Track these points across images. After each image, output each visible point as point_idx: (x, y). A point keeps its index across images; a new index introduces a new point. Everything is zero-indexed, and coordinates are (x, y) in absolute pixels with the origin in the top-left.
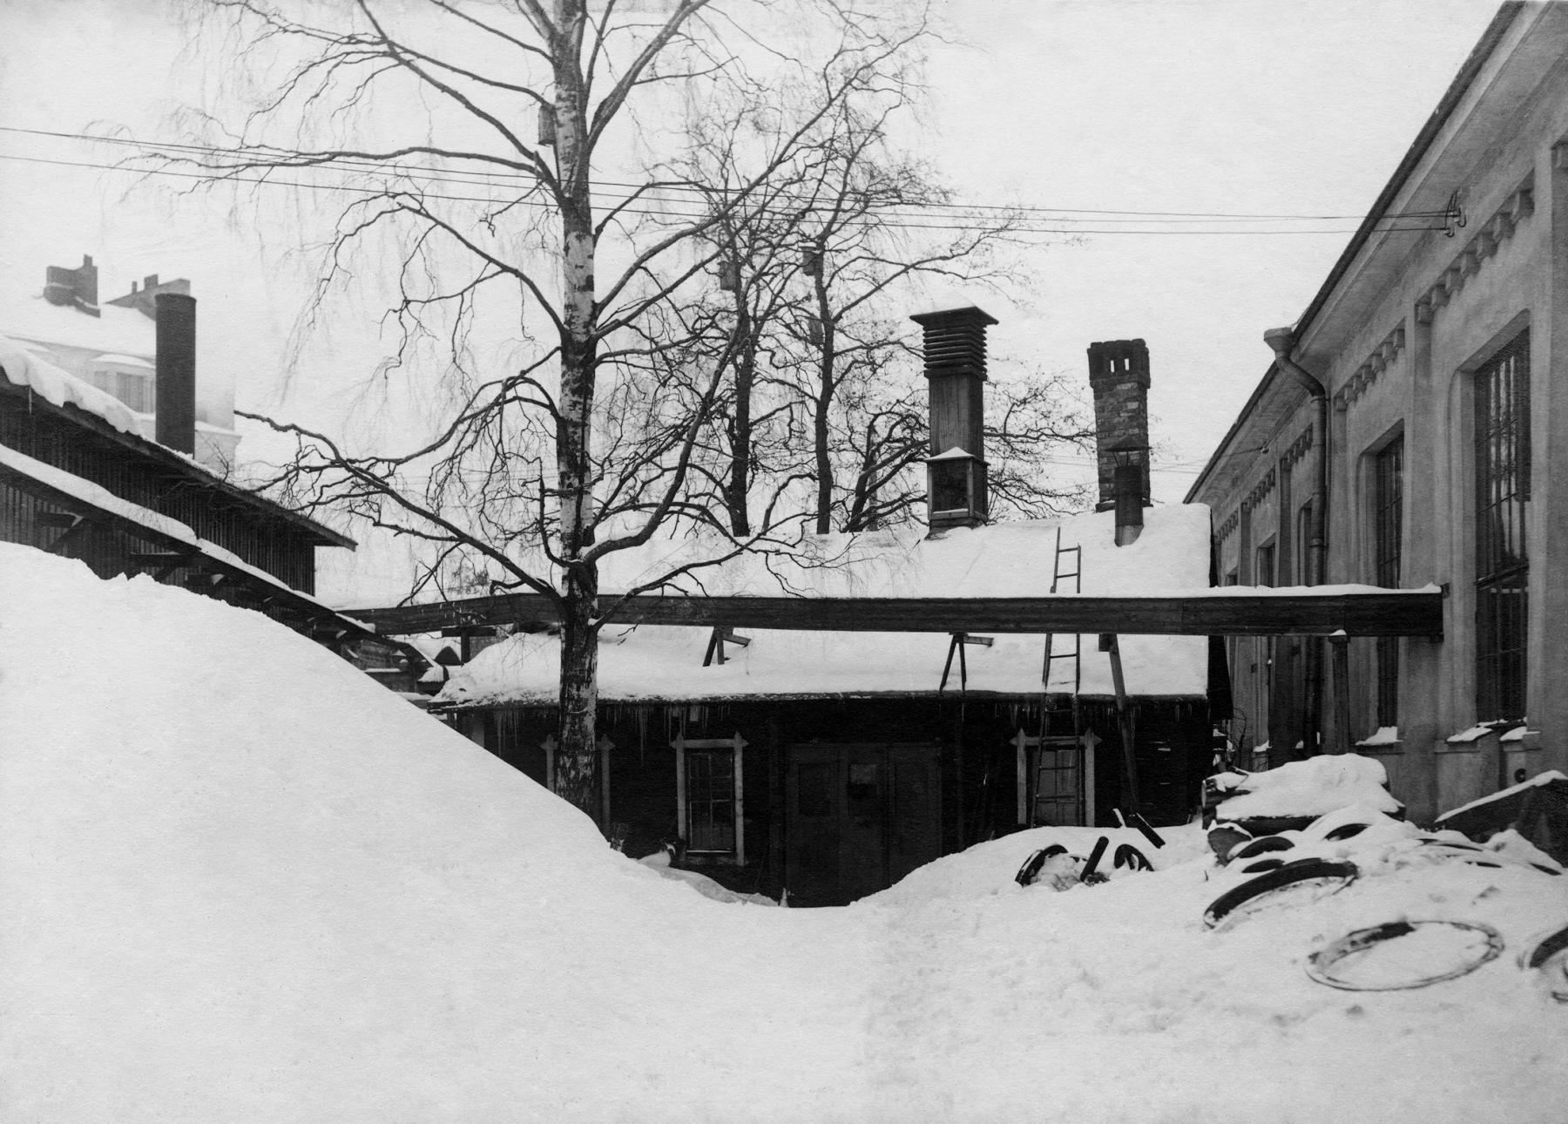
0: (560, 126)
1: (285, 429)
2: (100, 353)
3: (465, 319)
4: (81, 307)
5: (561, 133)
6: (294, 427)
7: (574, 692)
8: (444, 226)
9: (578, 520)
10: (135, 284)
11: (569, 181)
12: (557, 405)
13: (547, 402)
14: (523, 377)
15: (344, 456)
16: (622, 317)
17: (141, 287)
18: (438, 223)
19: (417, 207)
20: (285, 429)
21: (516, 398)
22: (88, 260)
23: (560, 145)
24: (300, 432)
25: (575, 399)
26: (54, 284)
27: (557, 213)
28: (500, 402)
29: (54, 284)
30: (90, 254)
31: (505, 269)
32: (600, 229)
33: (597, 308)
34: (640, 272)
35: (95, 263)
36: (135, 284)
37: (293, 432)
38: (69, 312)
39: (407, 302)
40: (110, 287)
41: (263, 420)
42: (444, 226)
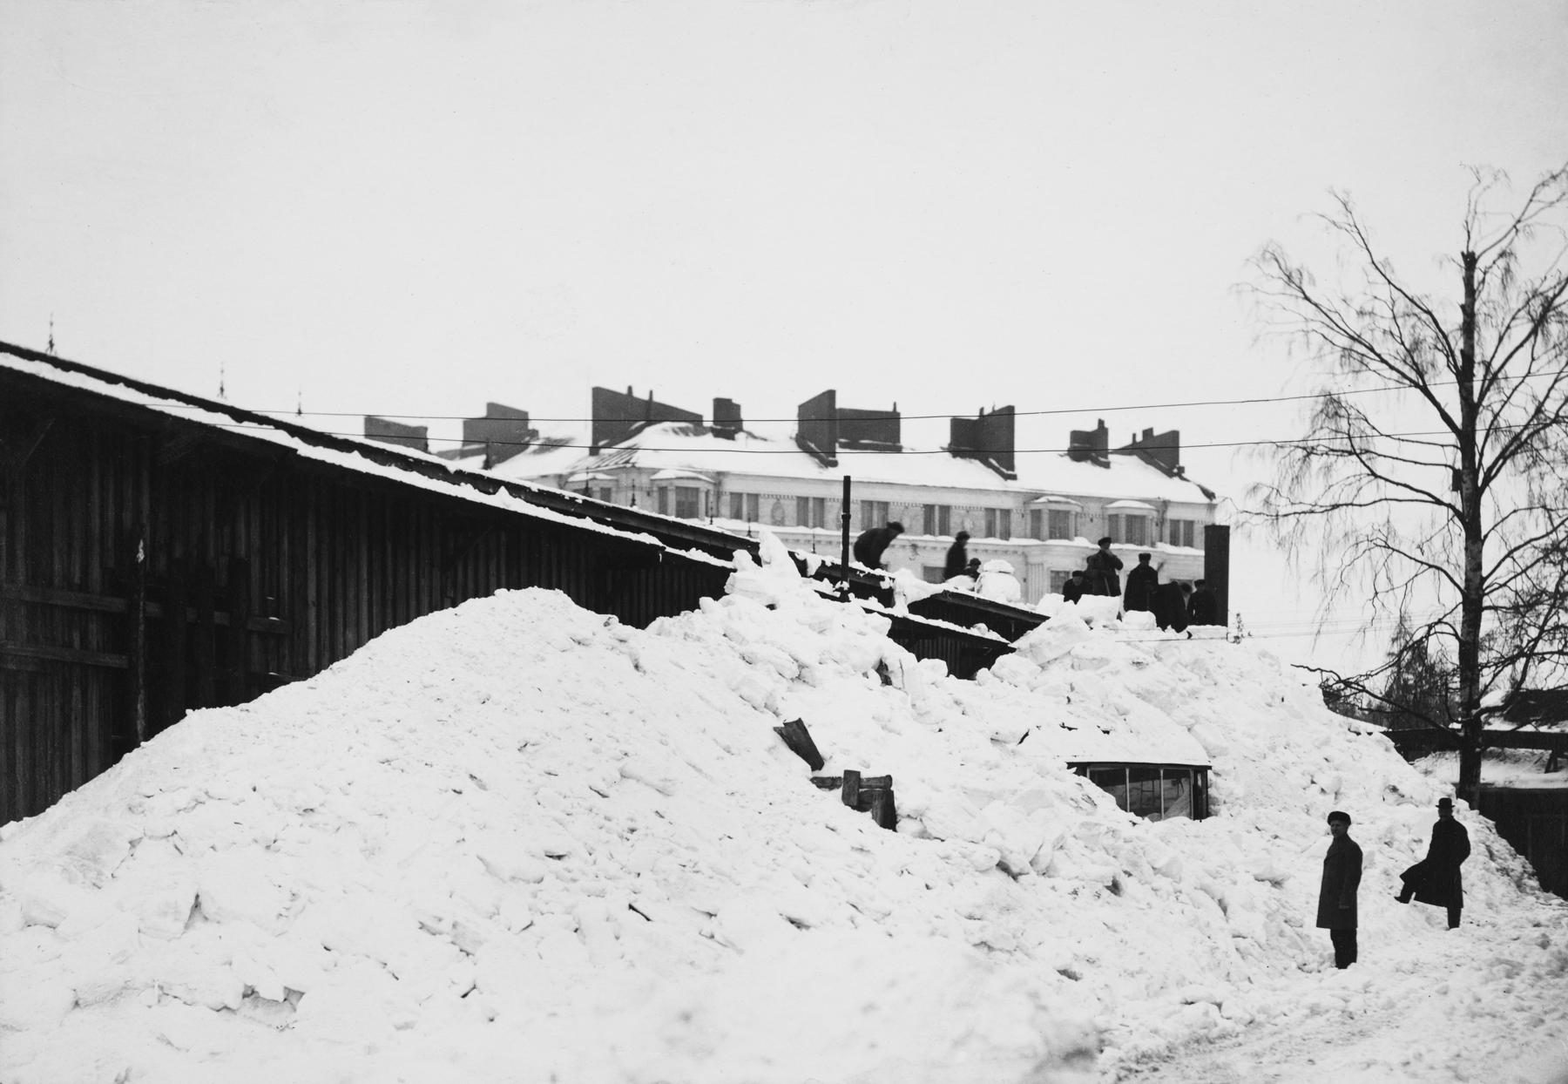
0: (1465, 482)
1: (1314, 671)
2: (1112, 501)
3: (1408, 598)
4: (1096, 462)
5: (1464, 486)
6: (1319, 669)
7: (1467, 788)
8: (1397, 551)
9: (1471, 695)
10: (1134, 436)
11: (1468, 512)
12: (1459, 633)
13: (1452, 632)
14: (1440, 621)
15: (1342, 678)
16: (1501, 581)
17: (1139, 438)
18: (1394, 550)
19: (1384, 544)
20: (1314, 671)
21: (1436, 633)
22: (1101, 423)
23: (1464, 490)
24: (1322, 671)
25: (1471, 630)
26: (1076, 445)
27: (1506, 378)
28: (1428, 635)
29: (1076, 445)
30: (1102, 419)
31: (1430, 566)
32: (1486, 536)
33: (1484, 579)
34: (1509, 560)
35: (1106, 425)
36: (1134, 436)
37: (1319, 671)
38: (1086, 467)
39: (1376, 593)
40: (1116, 440)
41: (1304, 667)
42: (1397, 551)
